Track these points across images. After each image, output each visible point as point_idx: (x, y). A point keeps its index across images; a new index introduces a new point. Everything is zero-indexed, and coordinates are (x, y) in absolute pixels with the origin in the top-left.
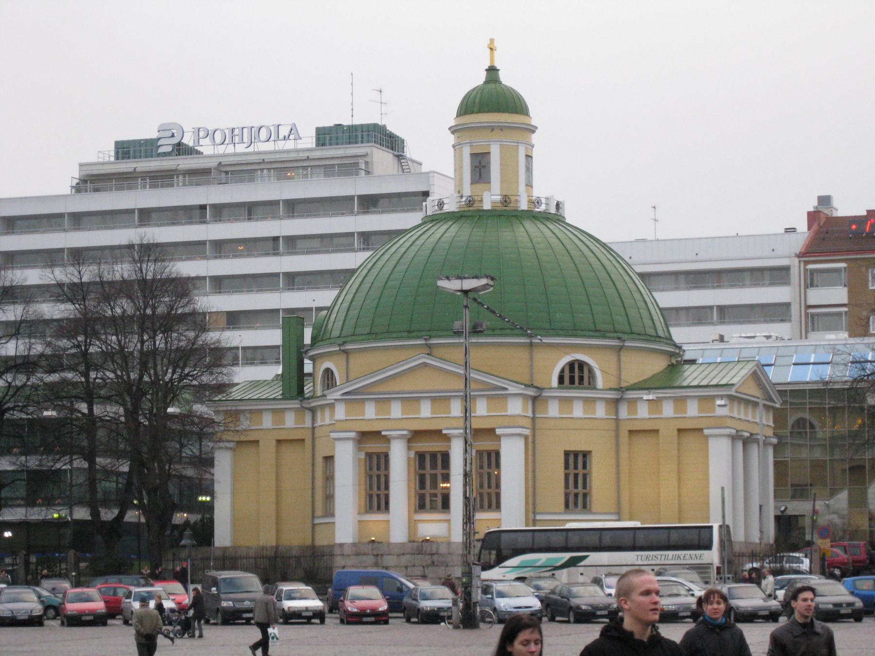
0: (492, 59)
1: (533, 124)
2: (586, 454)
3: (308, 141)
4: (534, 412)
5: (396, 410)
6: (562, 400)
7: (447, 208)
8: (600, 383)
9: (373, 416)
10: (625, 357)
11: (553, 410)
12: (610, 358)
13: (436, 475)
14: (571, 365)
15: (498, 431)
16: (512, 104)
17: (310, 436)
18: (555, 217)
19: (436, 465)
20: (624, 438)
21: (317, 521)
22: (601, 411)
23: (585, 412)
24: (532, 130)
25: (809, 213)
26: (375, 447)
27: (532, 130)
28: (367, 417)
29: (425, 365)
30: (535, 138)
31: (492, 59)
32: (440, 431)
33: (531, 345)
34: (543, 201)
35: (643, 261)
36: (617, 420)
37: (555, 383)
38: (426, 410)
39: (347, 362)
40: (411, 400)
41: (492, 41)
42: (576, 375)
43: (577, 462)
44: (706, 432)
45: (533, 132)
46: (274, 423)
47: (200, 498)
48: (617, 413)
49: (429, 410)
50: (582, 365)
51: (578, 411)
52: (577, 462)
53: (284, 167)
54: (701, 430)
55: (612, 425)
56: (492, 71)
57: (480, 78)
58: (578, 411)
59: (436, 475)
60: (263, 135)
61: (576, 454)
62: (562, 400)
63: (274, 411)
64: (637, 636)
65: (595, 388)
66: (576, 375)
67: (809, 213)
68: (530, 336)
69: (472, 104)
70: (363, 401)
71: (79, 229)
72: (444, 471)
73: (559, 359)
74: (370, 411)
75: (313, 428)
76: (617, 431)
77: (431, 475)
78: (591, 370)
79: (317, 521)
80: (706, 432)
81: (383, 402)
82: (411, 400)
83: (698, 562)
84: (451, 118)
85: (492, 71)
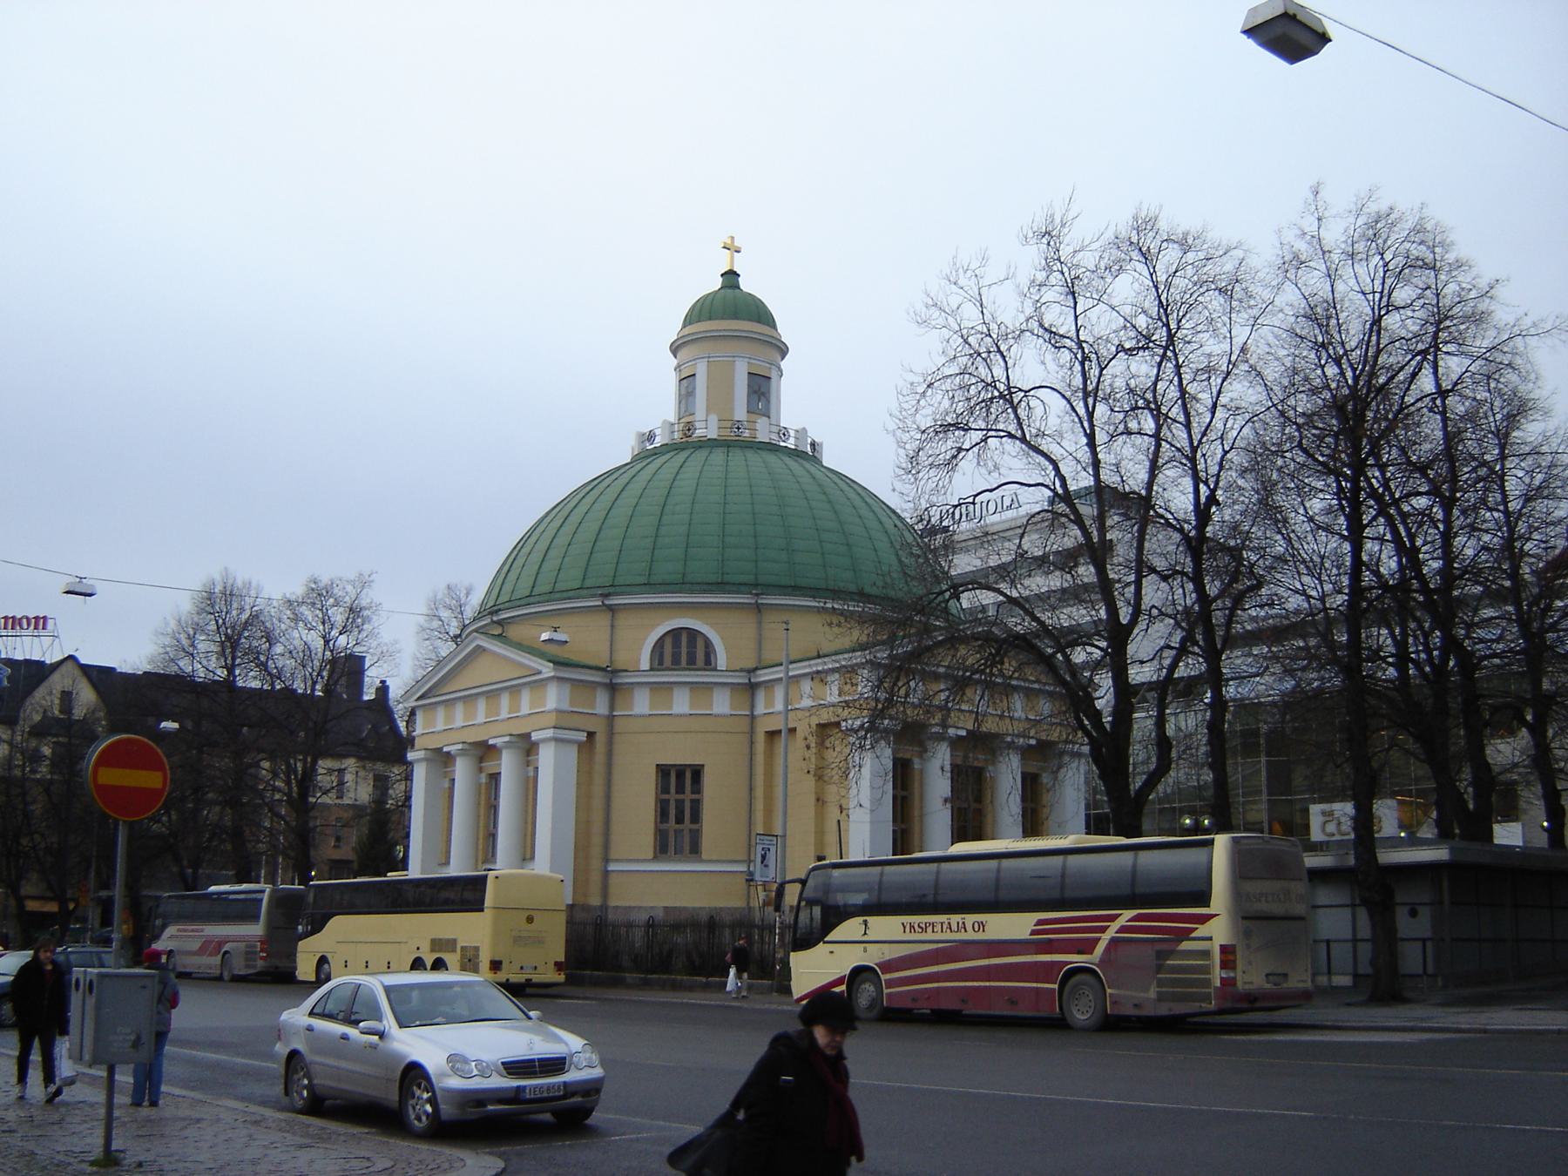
2: (697, 772)
4: (612, 707)
6: (654, 687)
8: (722, 661)
9: (647, 711)
10: (623, 620)
11: (641, 704)
12: (745, 626)
13: (668, 801)
14: (675, 633)
18: (809, 455)
21: (612, 867)
22: (721, 704)
23: (692, 706)
26: (978, 759)
28: (715, 711)
34: (792, 433)
36: (753, 717)
37: (645, 664)
42: (684, 651)
43: (680, 787)
47: (1471, 806)
48: (752, 707)
49: (647, 702)
50: (693, 634)
51: (681, 703)
52: (680, 787)
55: (744, 725)
56: (731, 276)
57: (716, 283)
58: (681, 703)
59: (668, 801)
61: (680, 771)
62: (654, 687)
66: (684, 651)
69: (702, 311)
72: (695, 796)
73: (654, 627)
76: (752, 732)
77: (692, 801)
78: (708, 644)
79: (612, 867)
83: (980, 936)
84: (673, 327)
85: (731, 276)
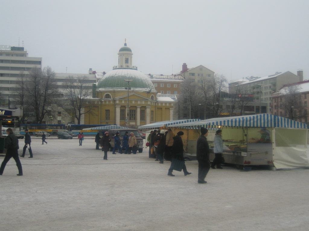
3: (9, 49)
8: (111, 98)
14: (107, 95)
15: (170, 109)
16: (129, 50)
19: (185, 116)
20: (156, 108)
24: (132, 54)
25: (95, 71)
27: (132, 54)
30: (133, 56)
35: (58, 77)
44: (147, 107)
50: (108, 94)
53: (8, 54)
54: (146, 107)
60: (3, 47)
64: (18, 150)
67: (95, 71)
69: (122, 50)
71: (2, 63)
80: (147, 107)
84: (118, 52)
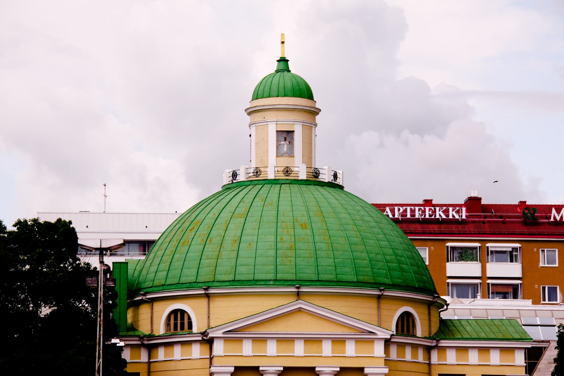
0: (283, 51)
1: (317, 107)
5: (272, 348)
7: (241, 178)
17: (146, 370)
29: (300, 310)
31: (283, 51)
32: (314, 368)
33: (379, 297)
38: (299, 349)
39: (209, 304)
40: (286, 340)
41: (283, 35)
45: (317, 114)
46: (166, 355)
48: (429, 359)
50: (183, 312)
63: (480, 349)
65: (191, 333)
68: (381, 290)
70: (240, 340)
74: (247, 348)
75: (149, 363)
81: (261, 340)
82: (286, 340)
85: (283, 60)
